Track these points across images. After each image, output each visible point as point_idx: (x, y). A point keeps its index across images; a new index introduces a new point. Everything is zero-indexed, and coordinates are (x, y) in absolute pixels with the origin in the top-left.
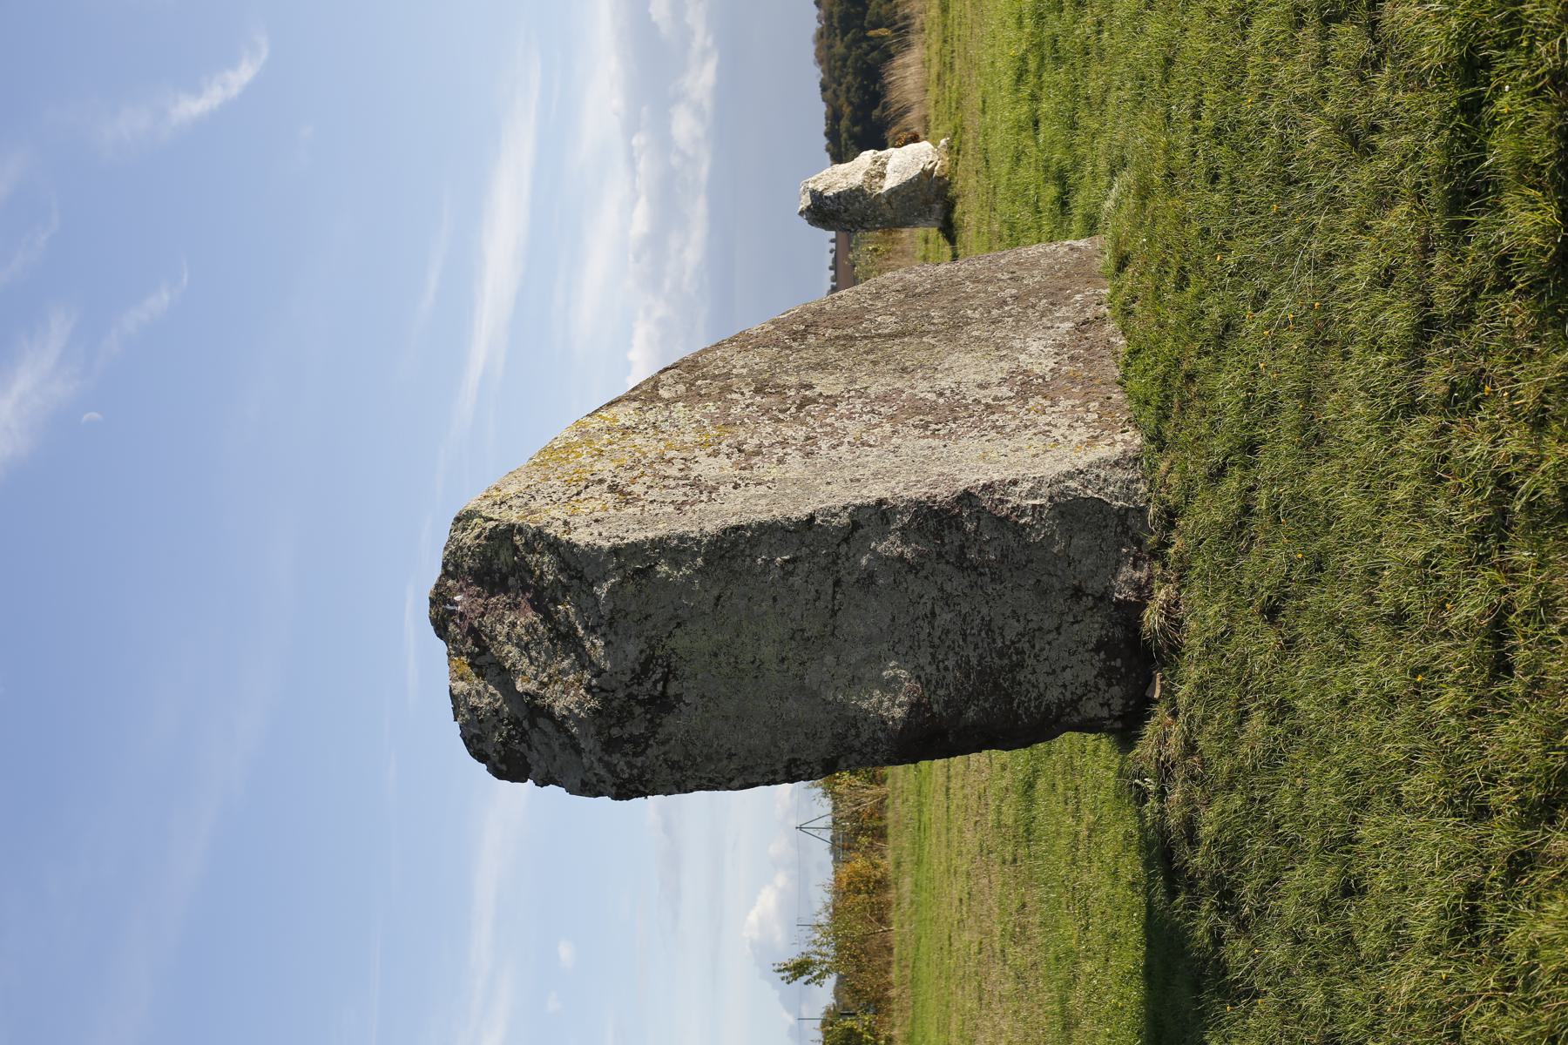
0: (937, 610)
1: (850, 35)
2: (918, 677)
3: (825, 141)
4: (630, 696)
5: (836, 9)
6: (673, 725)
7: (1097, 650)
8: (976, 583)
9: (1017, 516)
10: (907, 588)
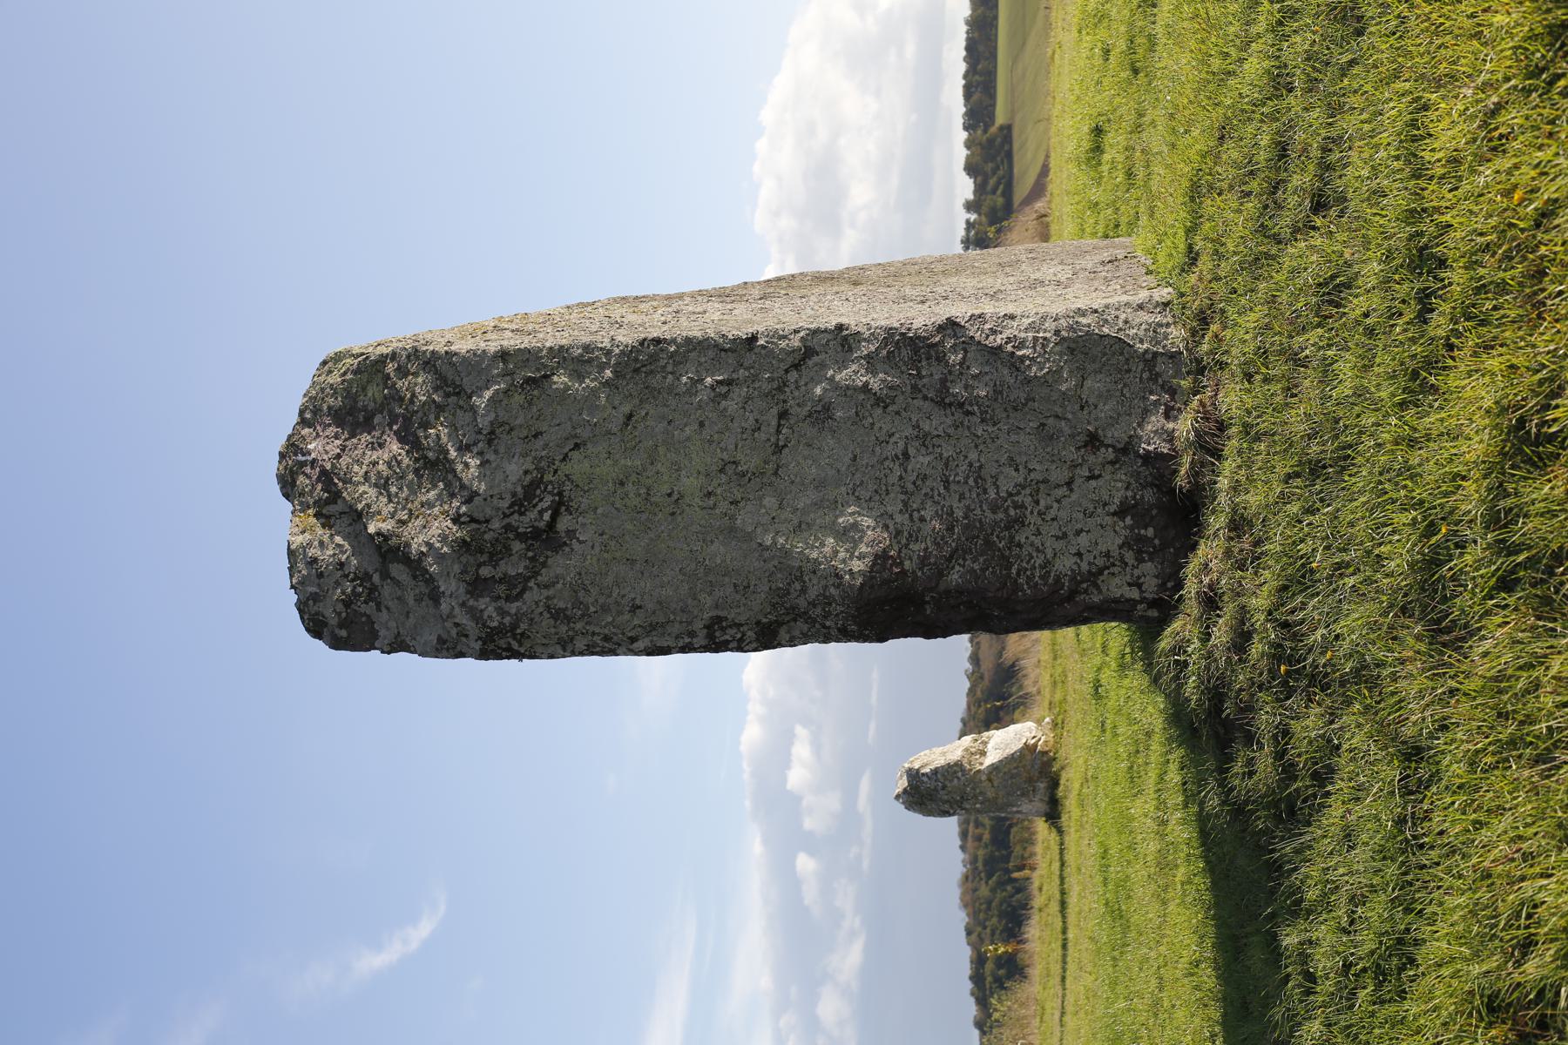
0: (912, 451)
1: (994, 878)
2: (886, 527)
3: (969, 985)
4: (508, 528)
5: (981, 853)
6: (560, 566)
7: (1121, 513)
8: (962, 423)
9: (1013, 347)
10: (873, 424)
